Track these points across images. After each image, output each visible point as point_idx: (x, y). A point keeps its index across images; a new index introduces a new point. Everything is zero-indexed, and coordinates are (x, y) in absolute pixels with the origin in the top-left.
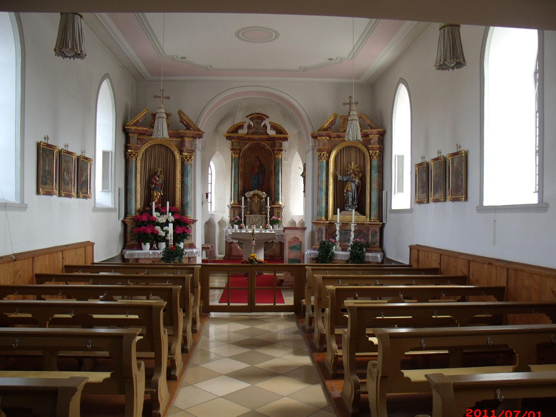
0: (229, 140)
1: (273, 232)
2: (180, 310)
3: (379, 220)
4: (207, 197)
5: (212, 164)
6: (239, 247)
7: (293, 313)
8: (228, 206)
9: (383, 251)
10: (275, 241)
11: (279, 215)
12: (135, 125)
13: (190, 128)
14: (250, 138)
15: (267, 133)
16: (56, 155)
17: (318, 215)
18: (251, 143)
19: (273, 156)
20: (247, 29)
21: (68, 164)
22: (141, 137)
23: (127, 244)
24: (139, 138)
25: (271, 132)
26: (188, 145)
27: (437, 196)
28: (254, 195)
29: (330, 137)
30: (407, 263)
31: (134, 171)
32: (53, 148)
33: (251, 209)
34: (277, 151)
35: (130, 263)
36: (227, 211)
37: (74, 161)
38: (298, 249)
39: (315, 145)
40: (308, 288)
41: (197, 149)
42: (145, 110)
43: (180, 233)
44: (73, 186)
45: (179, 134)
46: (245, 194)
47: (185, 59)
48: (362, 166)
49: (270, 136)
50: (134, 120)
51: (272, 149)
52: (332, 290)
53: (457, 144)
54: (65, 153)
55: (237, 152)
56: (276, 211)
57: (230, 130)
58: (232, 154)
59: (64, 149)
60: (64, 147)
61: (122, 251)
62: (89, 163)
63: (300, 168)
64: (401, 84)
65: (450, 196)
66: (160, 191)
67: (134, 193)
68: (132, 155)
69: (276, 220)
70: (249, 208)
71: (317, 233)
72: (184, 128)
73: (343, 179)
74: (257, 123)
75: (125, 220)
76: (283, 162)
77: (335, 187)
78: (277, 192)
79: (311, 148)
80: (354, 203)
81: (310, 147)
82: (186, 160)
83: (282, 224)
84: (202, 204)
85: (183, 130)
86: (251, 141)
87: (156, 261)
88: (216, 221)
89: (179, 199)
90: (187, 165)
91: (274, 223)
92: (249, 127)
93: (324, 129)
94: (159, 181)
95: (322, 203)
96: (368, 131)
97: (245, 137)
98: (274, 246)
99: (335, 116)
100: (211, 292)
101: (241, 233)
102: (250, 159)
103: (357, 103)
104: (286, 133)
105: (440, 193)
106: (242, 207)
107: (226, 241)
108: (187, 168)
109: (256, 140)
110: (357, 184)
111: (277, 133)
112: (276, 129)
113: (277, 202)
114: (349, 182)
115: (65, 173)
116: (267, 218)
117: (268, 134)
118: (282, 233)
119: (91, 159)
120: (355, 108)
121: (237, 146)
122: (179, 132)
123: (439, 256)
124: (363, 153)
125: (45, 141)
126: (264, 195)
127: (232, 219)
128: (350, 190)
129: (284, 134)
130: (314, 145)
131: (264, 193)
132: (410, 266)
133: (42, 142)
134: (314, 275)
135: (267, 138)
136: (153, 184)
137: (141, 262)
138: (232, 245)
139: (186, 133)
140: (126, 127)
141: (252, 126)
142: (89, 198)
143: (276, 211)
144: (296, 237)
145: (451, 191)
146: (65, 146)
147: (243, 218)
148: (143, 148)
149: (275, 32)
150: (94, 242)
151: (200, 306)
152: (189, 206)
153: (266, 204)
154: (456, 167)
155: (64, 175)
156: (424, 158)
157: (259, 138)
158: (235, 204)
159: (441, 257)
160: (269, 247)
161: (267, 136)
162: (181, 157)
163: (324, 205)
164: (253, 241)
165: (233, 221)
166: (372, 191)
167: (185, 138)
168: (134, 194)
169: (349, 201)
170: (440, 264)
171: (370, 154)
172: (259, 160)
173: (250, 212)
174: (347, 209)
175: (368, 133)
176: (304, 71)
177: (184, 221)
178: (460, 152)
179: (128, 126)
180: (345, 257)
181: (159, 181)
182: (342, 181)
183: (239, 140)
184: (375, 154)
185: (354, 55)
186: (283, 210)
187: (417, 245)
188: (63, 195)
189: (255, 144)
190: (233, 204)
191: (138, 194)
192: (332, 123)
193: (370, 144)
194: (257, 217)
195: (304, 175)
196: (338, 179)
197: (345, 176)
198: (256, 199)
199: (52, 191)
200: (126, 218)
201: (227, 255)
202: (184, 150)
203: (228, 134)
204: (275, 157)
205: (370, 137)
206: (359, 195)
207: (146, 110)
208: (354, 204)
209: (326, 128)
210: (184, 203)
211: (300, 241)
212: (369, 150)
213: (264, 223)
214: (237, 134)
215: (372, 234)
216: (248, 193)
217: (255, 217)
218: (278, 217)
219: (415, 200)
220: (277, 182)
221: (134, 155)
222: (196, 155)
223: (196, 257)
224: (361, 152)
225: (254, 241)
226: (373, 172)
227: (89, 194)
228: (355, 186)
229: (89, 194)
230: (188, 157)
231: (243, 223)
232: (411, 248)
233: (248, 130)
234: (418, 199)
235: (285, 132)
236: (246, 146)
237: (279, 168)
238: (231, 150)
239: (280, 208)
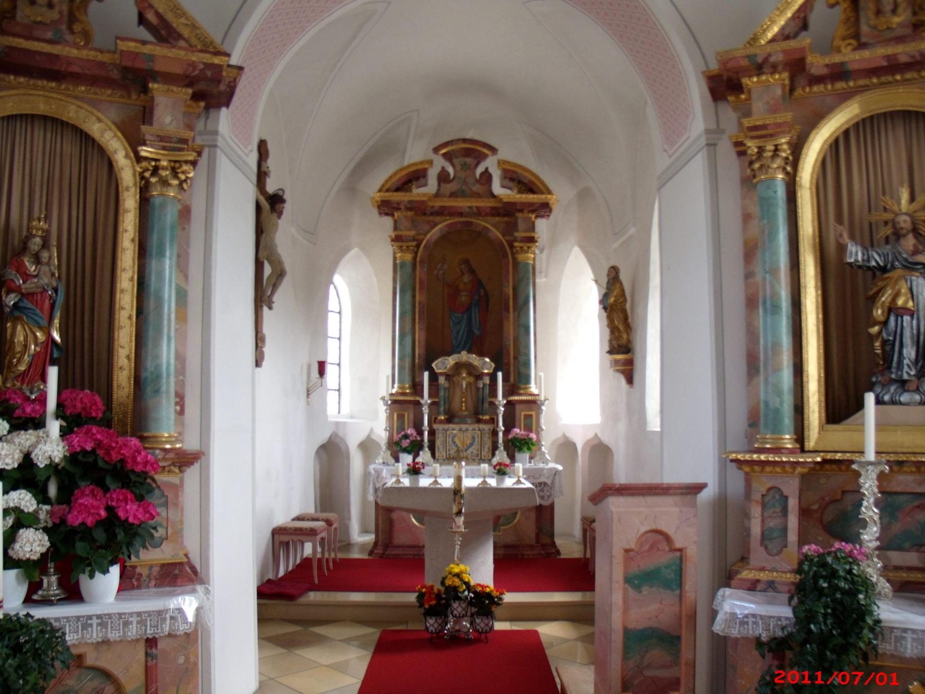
5: (337, 279)
6: (413, 520)
8: (383, 399)
11: (531, 424)
14: (444, 207)
19: (510, 256)
26: (168, 120)
28: (458, 366)
33: (450, 404)
34: (522, 241)
36: (382, 412)
38: (667, 585)
41: (218, 151)
43: (83, 524)
46: (433, 365)
51: (508, 238)
55: (408, 247)
56: (523, 413)
58: (395, 253)
69: (525, 439)
70: (444, 405)
73: (868, 261)
74: (465, 166)
78: (522, 359)
79: (703, 141)
82: (153, 180)
83: (540, 449)
84: (308, 395)
86: (448, 218)
88: (353, 442)
89: (128, 357)
90: (163, 206)
91: (517, 446)
92: (443, 177)
94: (36, 276)
95: (777, 370)
97: (431, 204)
101: (415, 490)
102: (445, 267)
106: (422, 402)
113: (523, 386)
114: (899, 272)
116: (495, 433)
121: (409, 230)
126: (486, 365)
127: (396, 438)
129: (542, 193)
130: (713, 126)
131: (486, 362)
135: (492, 208)
139: (152, 58)
141: (449, 174)
143: (521, 413)
144: (659, 527)
147: (426, 433)
152: (164, 388)
153: (494, 393)
157: (471, 208)
158: (404, 394)
161: (492, 200)
163: (787, 376)
164: (457, 519)
165: (398, 443)
172: (472, 271)
173: (447, 417)
177: (123, 461)
181: (36, 276)
182: (864, 268)
183: (413, 213)
186: (543, 408)
189: (460, 226)
194: (467, 430)
198: (464, 380)
201: (380, 543)
203: (382, 194)
204: (514, 259)
211: (678, 545)
213: (487, 447)
214: (408, 194)
216: (440, 360)
217: (460, 430)
218: (529, 428)
220: (522, 330)
225: (462, 519)
230: (165, 168)
231: (427, 449)
238: (397, 239)
239: (534, 404)
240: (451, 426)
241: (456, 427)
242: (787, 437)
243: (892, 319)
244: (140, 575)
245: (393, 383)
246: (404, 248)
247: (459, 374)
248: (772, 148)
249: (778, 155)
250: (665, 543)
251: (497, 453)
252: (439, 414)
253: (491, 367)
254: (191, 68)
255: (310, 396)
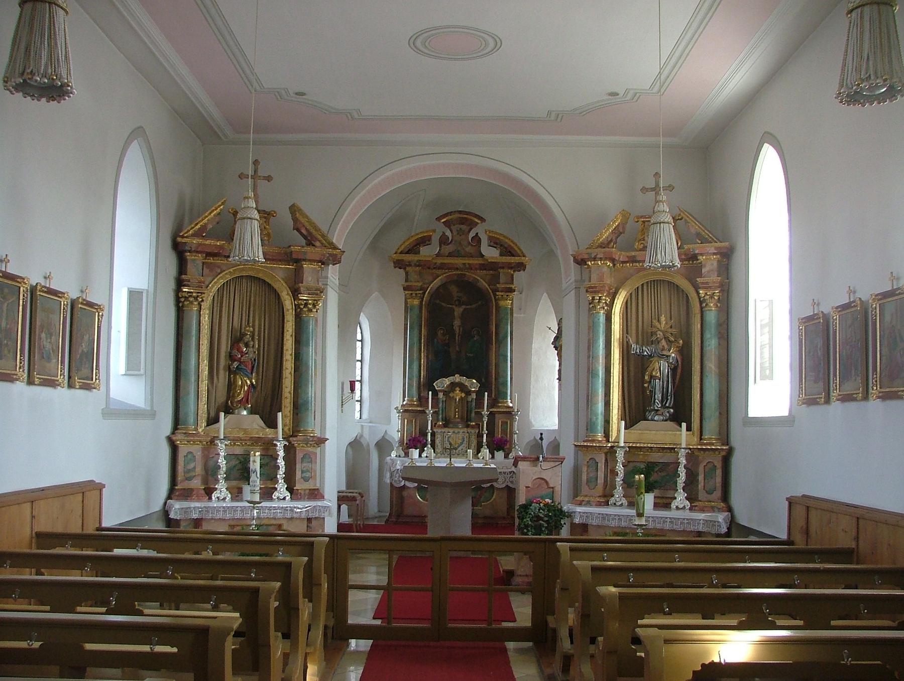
0: (400, 268)
1: (493, 466)
2: (277, 637)
3: (718, 439)
4: (352, 389)
5: (364, 320)
6: (418, 497)
7: (531, 644)
8: (396, 408)
9: (730, 509)
10: (495, 484)
12: (197, 234)
13: (315, 241)
15: (481, 253)
16: (24, 296)
17: (587, 430)
18: (447, 274)
20: (433, 32)
21: (51, 316)
22: (211, 260)
23: (176, 488)
24: (207, 263)
25: (491, 253)
27: (848, 388)
28: (453, 385)
29: (613, 260)
30: (784, 536)
31: (194, 332)
32: (18, 282)
35: (182, 528)
37: (64, 309)
39: (582, 278)
40: (562, 589)
41: (328, 286)
42: (220, 203)
44: (60, 361)
45: (291, 255)
47: (304, 97)
48: (682, 323)
49: (487, 260)
50: (197, 224)
51: (492, 287)
52: (612, 595)
53: (892, 273)
54: (43, 291)
55: (416, 294)
57: (403, 247)
59: (43, 284)
60: (44, 280)
61: (165, 503)
62: (97, 314)
63: (550, 329)
64: (766, 146)
65: (878, 389)
66: (250, 376)
67: (193, 378)
68: (191, 299)
71: (585, 469)
72: (304, 242)
73: (643, 352)
75: (173, 436)
76: (515, 315)
77: (626, 368)
78: (501, 380)
80: (666, 403)
81: (572, 283)
82: (305, 309)
84: (342, 405)
85: (298, 244)
87: (238, 526)
89: (290, 393)
90: (308, 322)
92: (443, 241)
93: (602, 243)
94: (246, 353)
96: (697, 248)
97: (434, 261)
98: (494, 497)
99: (623, 216)
100: (354, 596)
103: (670, 188)
104: (521, 255)
105: (855, 380)
107: (391, 483)
108: (308, 328)
109: (457, 269)
110: (671, 363)
111: (501, 255)
112: (501, 245)
114: (656, 359)
115: (43, 335)
116: (480, 436)
117: (482, 256)
118: (513, 469)
119: (100, 306)
120: (665, 198)
122: (291, 252)
123: (854, 520)
124: (685, 296)
125: (46, 282)
126: (473, 384)
128: (658, 375)
132: (789, 542)
133: (39, 285)
134: (575, 562)
136: (235, 360)
137: (206, 527)
138: (405, 494)
139: (305, 253)
140: (179, 239)
142: (95, 388)
145: (878, 376)
146: (45, 278)
148: (216, 283)
149: (493, 38)
150: (103, 483)
151: (326, 627)
152: (310, 408)
154: (891, 322)
155: (40, 338)
156: (818, 305)
157: (464, 264)
159: (858, 524)
160: (483, 497)
162: (296, 303)
166: (705, 378)
167: (304, 263)
168: (195, 381)
169: (655, 399)
170: (857, 539)
171: (699, 298)
174: (650, 418)
175: (697, 252)
176: (556, 120)
178: (898, 289)
179: (183, 237)
180: (664, 522)
181: (246, 353)
184: (712, 297)
185: (661, 87)
187: (804, 496)
188: (37, 381)
190: (406, 404)
191: (202, 381)
192: (618, 232)
193: (701, 276)
194: (459, 432)
195: (557, 344)
196: (632, 352)
197: (648, 345)
198: (458, 394)
199: (13, 372)
200: (176, 431)
202: (302, 289)
204: (497, 305)
205: (699, 261)
206: (677, 381)
207: (223, 204)
208: (667, 405)
209: (606, 242)
210: (300, 401)
211: (551, 486)
212: (700, 288)
215: (706, 470)
217: (454, 432)
219: (799, 397)
220: (501, 358)
221: (196, 298)
222: (326, 299)
223: (324, 518)
224: (681, 294)
226: (707, 335)
227: (96, 379)
228: (668, 366)
229: (94, 379)
230: (310, 304)
232: (791, 502)
233: (440, 247)
234: (805, 395)
235: (518, 251)
236: (436, 283)
237: (508, 328)
238: (405, 289)
240: (446, 430)
241: (451, 430)
242: (600, 435)
243: (652, 380)
244: (301, 493)
245: (404, 397)
246: (414, 295)
247: (453, 391)
248: (598, 298)
249: (600, 302)
250: (545, 484)
251: (482, 450)
252: (438, 420)
253: (477, 386)
254: (323, 257)
255: (343, 406)
